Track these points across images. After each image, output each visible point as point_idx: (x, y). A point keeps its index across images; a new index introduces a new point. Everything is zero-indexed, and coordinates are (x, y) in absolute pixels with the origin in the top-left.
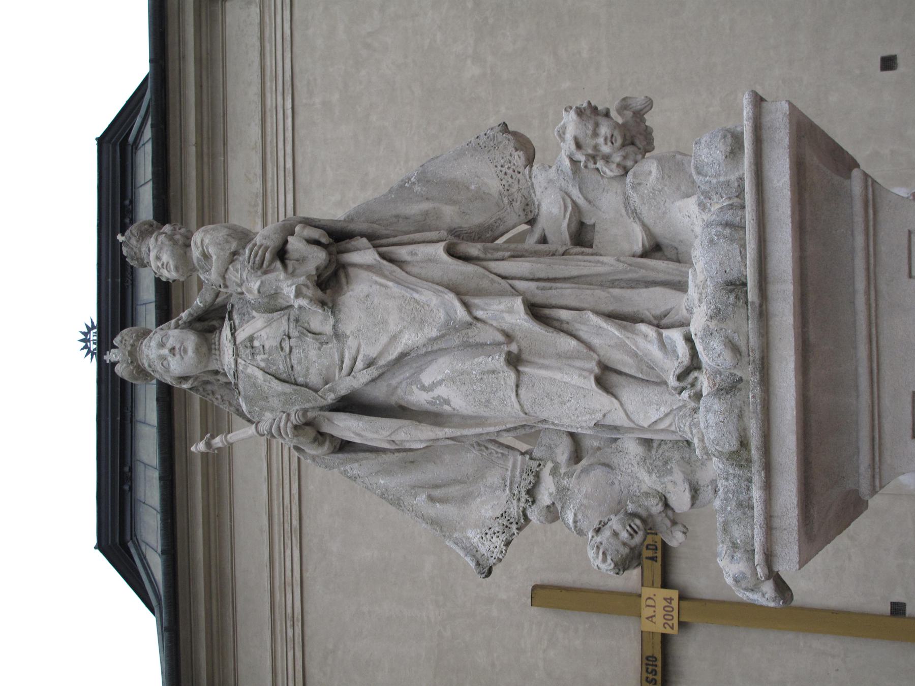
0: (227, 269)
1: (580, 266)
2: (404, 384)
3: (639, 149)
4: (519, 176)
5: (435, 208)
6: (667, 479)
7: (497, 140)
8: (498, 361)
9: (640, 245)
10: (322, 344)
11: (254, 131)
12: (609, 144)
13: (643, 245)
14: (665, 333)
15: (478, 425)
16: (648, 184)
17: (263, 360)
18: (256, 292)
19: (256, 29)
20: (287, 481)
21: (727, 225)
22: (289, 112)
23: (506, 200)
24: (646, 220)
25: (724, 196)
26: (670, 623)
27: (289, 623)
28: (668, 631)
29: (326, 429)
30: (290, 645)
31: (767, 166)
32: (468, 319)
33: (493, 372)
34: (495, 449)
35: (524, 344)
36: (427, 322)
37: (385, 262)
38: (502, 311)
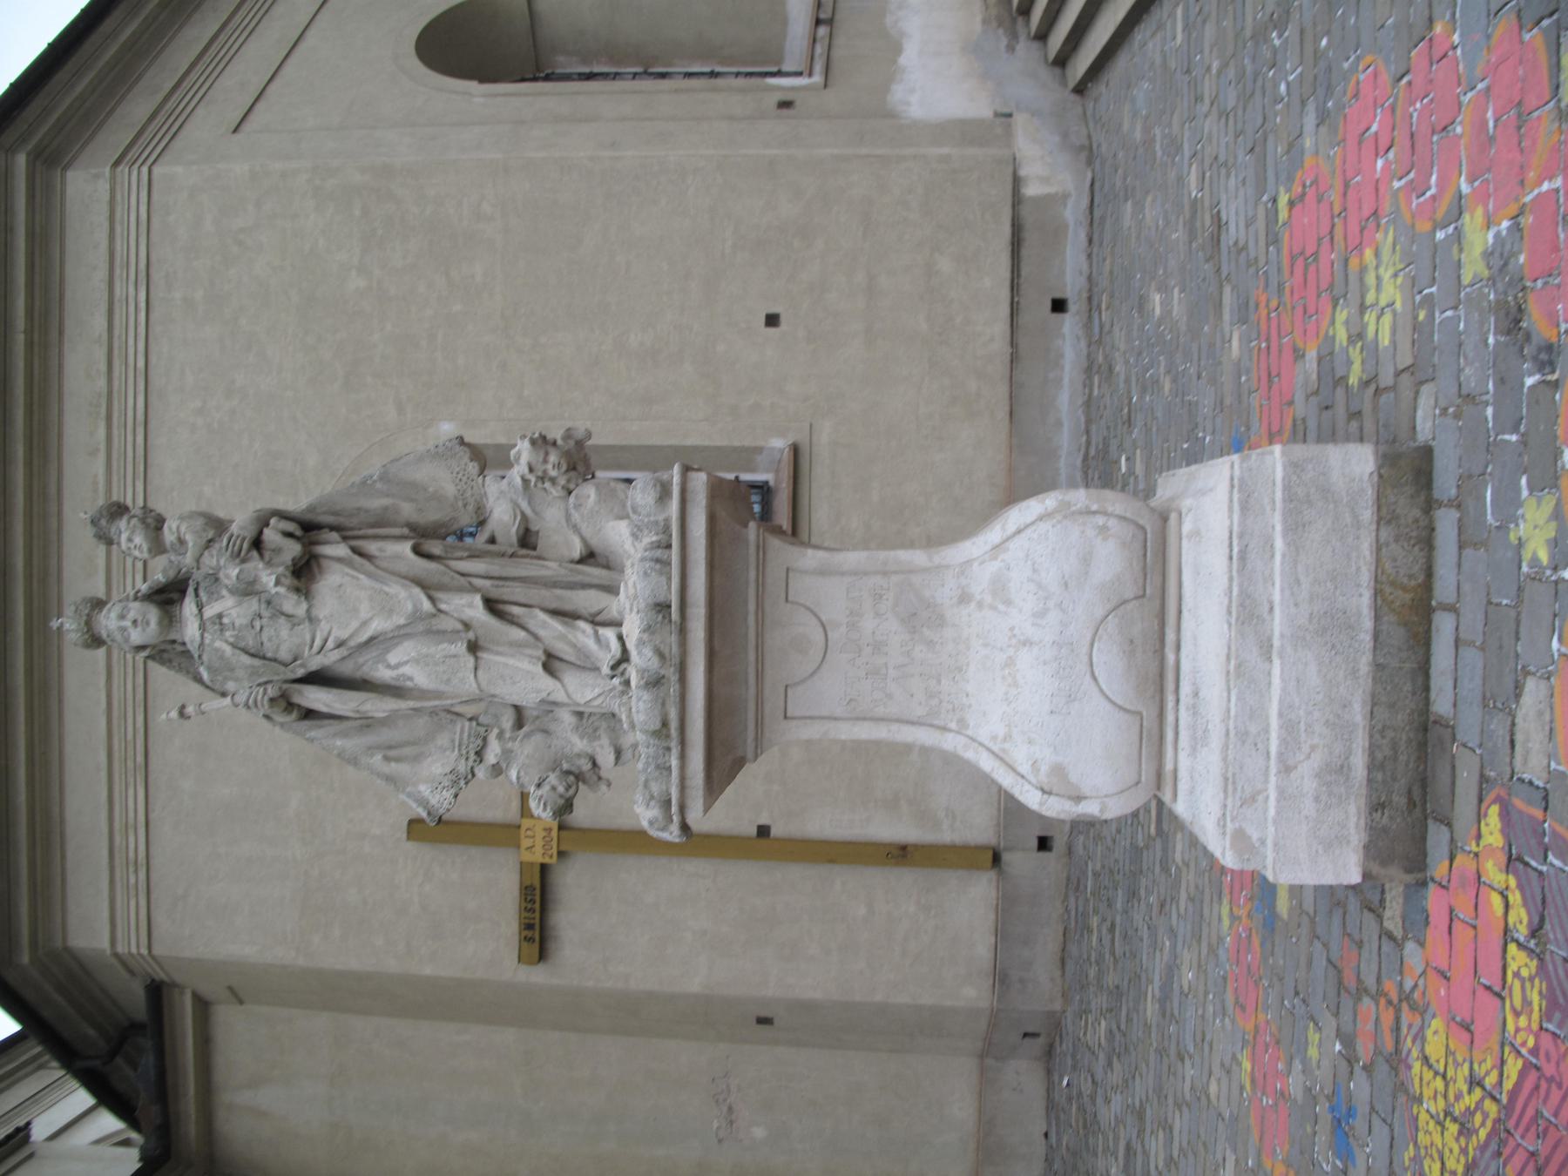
0: (201, 555)
2: (370, 663)
6: (596, 743)
8: (460, 648)
9: (578, 552)
10: (294, 625)
11: (100, 323)
14: (602, 631)
17: (232, 636)
18: (234, 578)
19: (105, 208)
20: (130, 714)
21: (658, 561)
22: (143, 305)
23: (460, 504)
24: (584, 534)
26: (550, 852)
27: (131, 869)
28: (547, 860)
29: (296, 699)
30: (132, 892)
31: (689, 520)
32: (433, 610)
33: (455, 656)
38: (463, 606)
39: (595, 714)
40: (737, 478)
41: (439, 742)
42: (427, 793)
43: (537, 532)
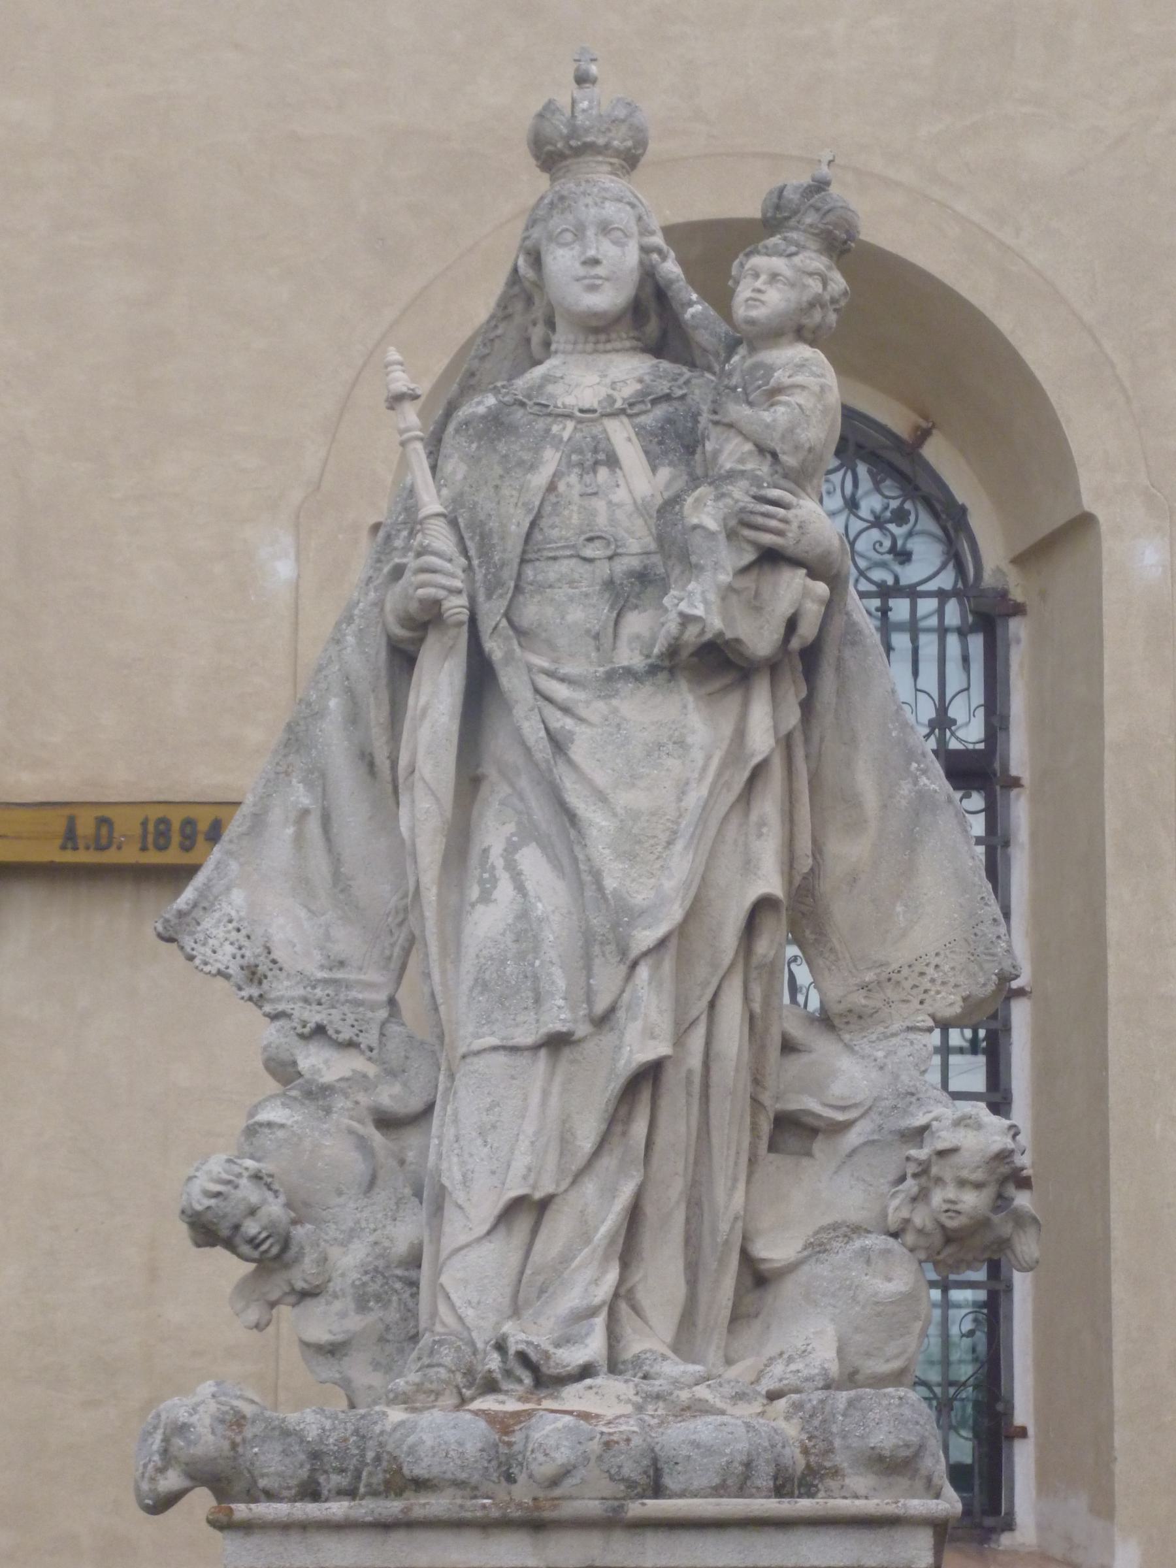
0: (746, 438)
1: (728, 1148)
3: (938, 1253)
4: (916, 1002)
5: (866, 821)
7: (988, 961)
10: (597, 637)
12: (945, 1207)
13: (764, 1260)
14: (600, 1322)
15: (444, 950)
16: (867, 1278)
23: (869, 976)
25: (812, 1443)
32: (634, 953)
34: (400, 941)
35: (590, 1047)
36: (632, 867)
37: (746, 774)
39: (415, 1295)
40: (1023, 1433)
41: (339, 932)
42: (227, 909)
43: (809, 1154)
